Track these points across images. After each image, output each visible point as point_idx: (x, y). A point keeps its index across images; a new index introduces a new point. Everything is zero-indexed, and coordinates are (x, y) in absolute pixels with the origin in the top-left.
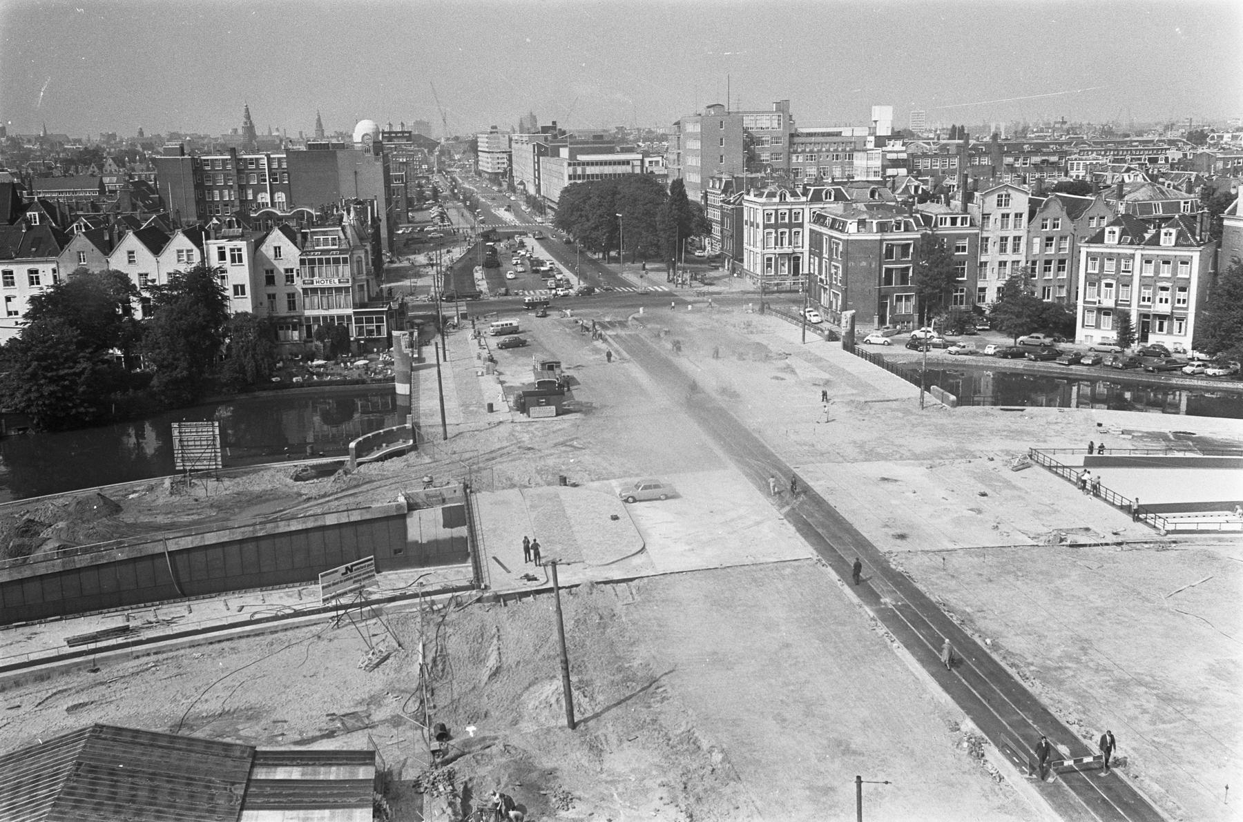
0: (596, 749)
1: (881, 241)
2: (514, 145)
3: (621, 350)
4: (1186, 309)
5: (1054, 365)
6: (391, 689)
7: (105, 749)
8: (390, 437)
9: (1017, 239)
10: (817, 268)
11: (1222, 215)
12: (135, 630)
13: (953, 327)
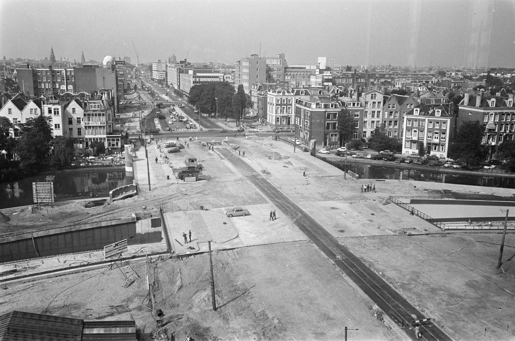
0: (226, 319)
1: (325, 112)
2: (168, 68)
3: (220, 154)
4: (445, 141)
5: (394, 163)
6: (136, 295)
7: (20, 322)
8: (126, 189)
9: (379, 112)
10: (299, 122)
11: (458, 105)
12: (20, 271)
13: (354, 147)
